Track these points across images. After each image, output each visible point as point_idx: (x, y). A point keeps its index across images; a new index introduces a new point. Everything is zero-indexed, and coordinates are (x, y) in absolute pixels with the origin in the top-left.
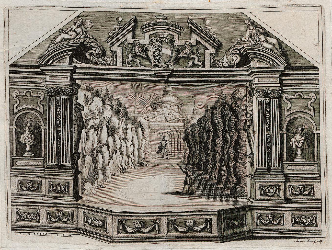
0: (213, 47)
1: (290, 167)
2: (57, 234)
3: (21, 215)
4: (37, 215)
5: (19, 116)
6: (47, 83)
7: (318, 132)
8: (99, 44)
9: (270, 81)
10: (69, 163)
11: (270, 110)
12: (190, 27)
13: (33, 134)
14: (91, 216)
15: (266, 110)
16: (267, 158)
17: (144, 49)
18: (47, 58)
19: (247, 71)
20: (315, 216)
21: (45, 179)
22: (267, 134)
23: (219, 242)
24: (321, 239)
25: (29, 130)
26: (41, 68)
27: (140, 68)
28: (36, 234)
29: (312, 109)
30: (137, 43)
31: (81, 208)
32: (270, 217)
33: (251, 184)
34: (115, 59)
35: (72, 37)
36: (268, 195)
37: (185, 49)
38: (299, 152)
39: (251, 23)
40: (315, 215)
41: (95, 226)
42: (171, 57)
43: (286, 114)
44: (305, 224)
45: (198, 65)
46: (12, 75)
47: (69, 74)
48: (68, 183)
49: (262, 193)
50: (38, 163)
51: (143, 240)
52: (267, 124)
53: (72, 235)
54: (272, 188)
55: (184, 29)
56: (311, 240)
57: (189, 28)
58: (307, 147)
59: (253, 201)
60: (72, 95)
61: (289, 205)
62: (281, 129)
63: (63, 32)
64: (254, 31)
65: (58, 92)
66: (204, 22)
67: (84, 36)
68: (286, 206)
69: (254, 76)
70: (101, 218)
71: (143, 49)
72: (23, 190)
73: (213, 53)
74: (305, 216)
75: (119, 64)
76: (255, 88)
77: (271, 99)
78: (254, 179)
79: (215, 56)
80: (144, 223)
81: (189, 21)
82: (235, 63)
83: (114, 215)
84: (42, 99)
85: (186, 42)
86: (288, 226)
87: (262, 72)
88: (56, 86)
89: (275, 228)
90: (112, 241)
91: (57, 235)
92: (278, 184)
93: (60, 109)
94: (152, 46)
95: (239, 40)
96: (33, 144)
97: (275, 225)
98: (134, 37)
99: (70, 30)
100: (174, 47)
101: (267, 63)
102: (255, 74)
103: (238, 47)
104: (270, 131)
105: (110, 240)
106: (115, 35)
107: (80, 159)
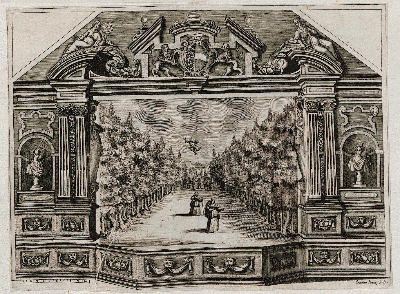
0: (256, 50)
1: (348, 195)
2: (71, 279)
3: (27, 259)
4: (45, 260)
5: (25, 143)
6: (59, 101)
7: (381, 152)
8: (121, 52)
9: (323, 91)
10: (86, 195)
11: (323, 126)
12: (228, 26)
13: (42, 163)
14: (112, 258)
15: (319, 126)
16: (321, 184)
17: (174, 55)
18: (58, 71)
19: (296, 78)
20: (377, 253)
21: (56, 216)
22: (320, 155)
23: (264, 285)
24: (384, 279)
25: (37, 159)
26: (51, 84)
27: (170, 78)
28: (45, 281)
29: (374, 126)
30: (166, 48)
31: (100, 249)
32: (325, 255)
33: (302, 216)
34: (139, 69)
35: (89, 45)
36: (322, 230)
37: (223, 53)
38: (359, 176)
39: (301, 23)
40: (377, 251)
41: (117, 270)
42: (205, 63)
43: (343, 130)
44: (365, 262)
45: (238, 72)
46: (16, 94)
47: (85, 90)
48: (83, 219)
49: (315, 227)
50: (48, 197)
51: (174, 283)
52: (321, 143)
53: (88, 281)
54: (327, 220)
55: (221, 29)
56: (372, 280)
57: (227, 27)
58: (368, 170)
59: (305, 236)
60: (88, 114)
61: (347, 240)
62: (337, 149)
63: (78, 38)
64: (305, 32)
65: (71, 111)
66: (244, 20)
67: (102, 43)
68: (344, 241)
69: (304, 85)
70: (124, 260)
71: (173, 55)
72: (29, 230)
73: (256, 57)
74: (366, 253)
75: (145, 75)
76: (305, 99)
77: (325, 113)
78: (306, 211)
79: (257, 61)
80: (175, 262)
81: (226, 19)
82: (282, 69)
83: (139, 255)
84: (52, 121)
85: (223, 44)
86: (346, 265)
87: (314, 80)
88: (69, 104)
89: (330, 267)
90: (138, 285)
91: (70, 281)
92: (334, 215)
93: (74, 132)
94: (183, 51)
95: (286, 41)
96: (42, 176)
97: (331, 264)
98: (161, 41)
99: (86, 36)
100: (209, 51)
101: (320, 70)
102: (306, 82)
103: (285, 50)
104: (324, 151)
105: (135, 285)
106: (139, 39)
107: (99, 191)
